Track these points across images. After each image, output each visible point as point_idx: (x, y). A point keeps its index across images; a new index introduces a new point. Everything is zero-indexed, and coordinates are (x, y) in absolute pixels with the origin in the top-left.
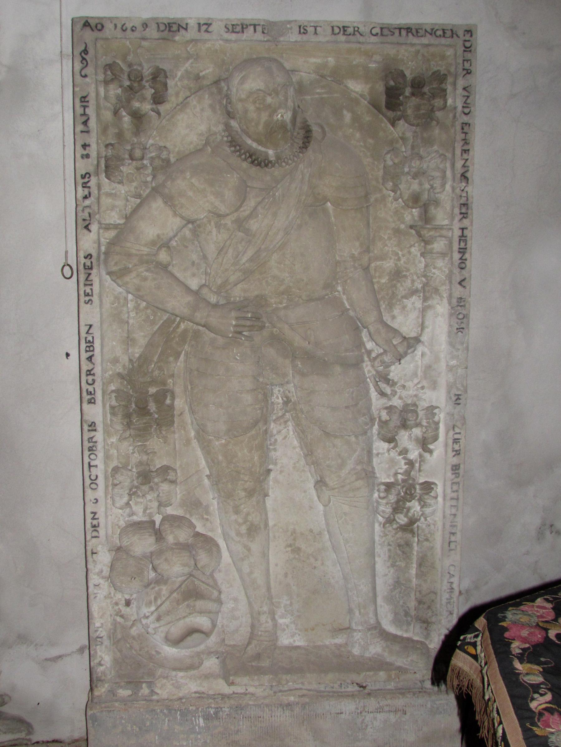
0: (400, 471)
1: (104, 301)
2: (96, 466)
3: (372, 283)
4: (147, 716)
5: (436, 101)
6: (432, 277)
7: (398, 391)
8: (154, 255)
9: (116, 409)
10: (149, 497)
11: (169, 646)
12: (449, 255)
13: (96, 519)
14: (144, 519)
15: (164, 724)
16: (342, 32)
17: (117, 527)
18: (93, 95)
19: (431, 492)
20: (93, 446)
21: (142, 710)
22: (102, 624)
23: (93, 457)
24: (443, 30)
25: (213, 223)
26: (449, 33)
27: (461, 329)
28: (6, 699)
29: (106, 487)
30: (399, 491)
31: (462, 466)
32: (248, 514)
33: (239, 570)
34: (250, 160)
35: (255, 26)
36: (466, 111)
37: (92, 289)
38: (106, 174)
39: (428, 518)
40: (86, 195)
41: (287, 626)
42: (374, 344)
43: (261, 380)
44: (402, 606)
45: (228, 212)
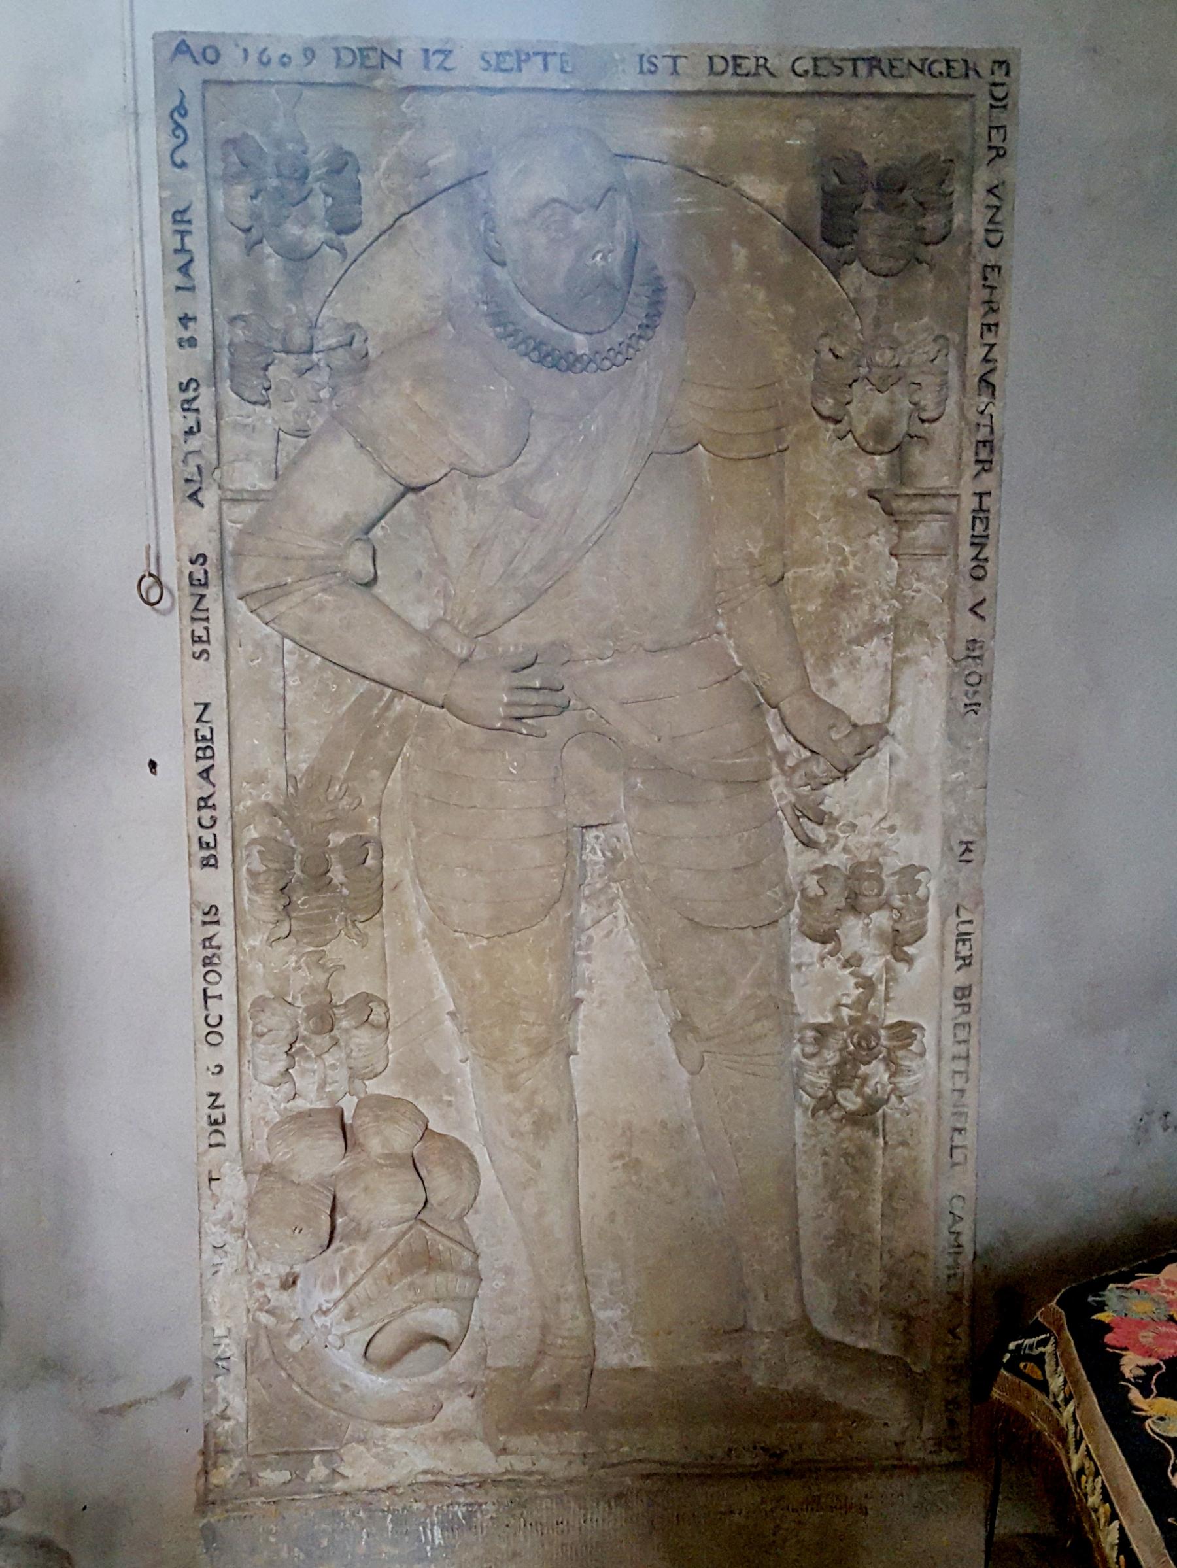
0: (845, 1001)
1: (233, 654)
2: (220, 997)
3: (788, 612)
4: (324, 1526)
5: (929, 218)
6: (913, 598)
7: (841, 835)
8: (340, 558)
9: (261, 879)
10: (329, 1059)
11: (370, 1372)
12: (951, 552)
13: (217, 1107)
14: (319, 1105)
15: (359, 1543)
16: (730, 70)
17: (262, 1123)
18: (199, 208)
19: (910, 1044)
20: (214, 955)
21: (312, 1513)
22: (229, 1330)
23: (212, 977)
24: (948, 61)
25: (459, 489)
26: (959, 67)
27: (973, 707)
28: (14, 1500)
29: (240, 1039)
30: (845, 1041)
31: (975, 990)
32: (534, 1092)
33: (517, 1210)
34: (535, 355)
35: (545, 55)
36: (994, 238)
37: (207, 629)
38: (232, 381)
39: (905, 1099)
40: (191, 428)
41: (616, 1325)
42: (792, 740)
43: (561, 815)
44: (854, 1282)
45: (492, 467)
